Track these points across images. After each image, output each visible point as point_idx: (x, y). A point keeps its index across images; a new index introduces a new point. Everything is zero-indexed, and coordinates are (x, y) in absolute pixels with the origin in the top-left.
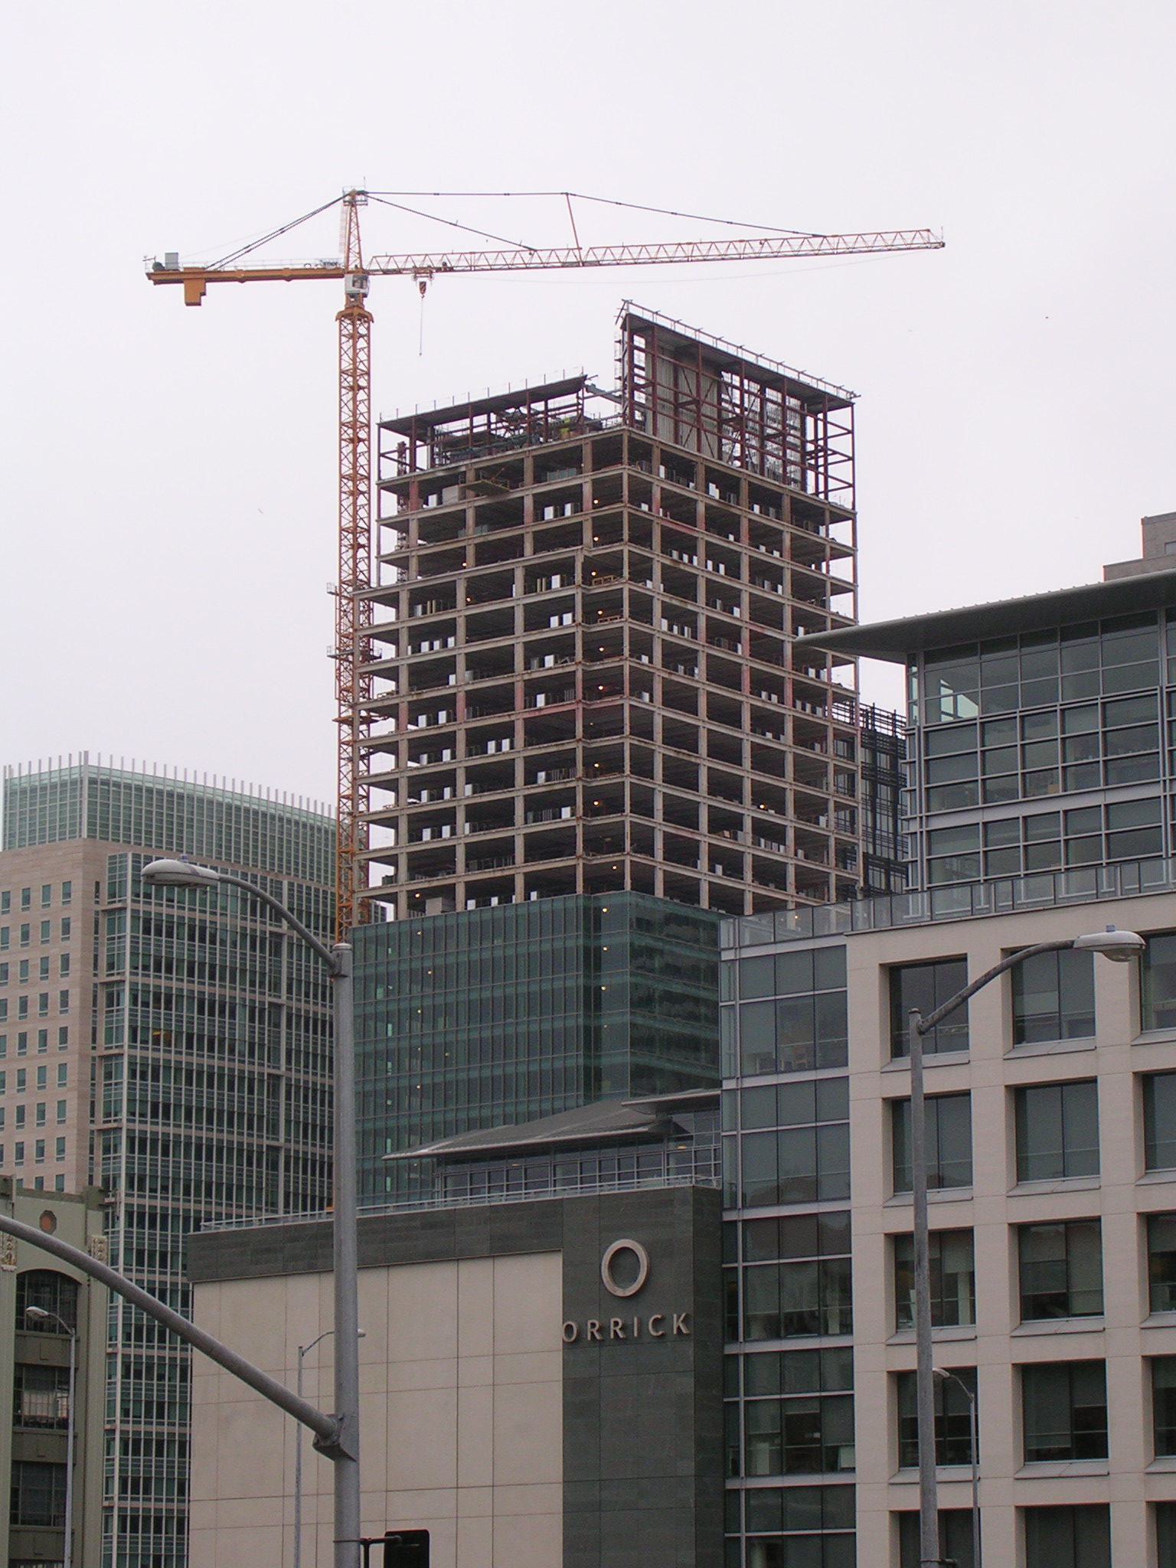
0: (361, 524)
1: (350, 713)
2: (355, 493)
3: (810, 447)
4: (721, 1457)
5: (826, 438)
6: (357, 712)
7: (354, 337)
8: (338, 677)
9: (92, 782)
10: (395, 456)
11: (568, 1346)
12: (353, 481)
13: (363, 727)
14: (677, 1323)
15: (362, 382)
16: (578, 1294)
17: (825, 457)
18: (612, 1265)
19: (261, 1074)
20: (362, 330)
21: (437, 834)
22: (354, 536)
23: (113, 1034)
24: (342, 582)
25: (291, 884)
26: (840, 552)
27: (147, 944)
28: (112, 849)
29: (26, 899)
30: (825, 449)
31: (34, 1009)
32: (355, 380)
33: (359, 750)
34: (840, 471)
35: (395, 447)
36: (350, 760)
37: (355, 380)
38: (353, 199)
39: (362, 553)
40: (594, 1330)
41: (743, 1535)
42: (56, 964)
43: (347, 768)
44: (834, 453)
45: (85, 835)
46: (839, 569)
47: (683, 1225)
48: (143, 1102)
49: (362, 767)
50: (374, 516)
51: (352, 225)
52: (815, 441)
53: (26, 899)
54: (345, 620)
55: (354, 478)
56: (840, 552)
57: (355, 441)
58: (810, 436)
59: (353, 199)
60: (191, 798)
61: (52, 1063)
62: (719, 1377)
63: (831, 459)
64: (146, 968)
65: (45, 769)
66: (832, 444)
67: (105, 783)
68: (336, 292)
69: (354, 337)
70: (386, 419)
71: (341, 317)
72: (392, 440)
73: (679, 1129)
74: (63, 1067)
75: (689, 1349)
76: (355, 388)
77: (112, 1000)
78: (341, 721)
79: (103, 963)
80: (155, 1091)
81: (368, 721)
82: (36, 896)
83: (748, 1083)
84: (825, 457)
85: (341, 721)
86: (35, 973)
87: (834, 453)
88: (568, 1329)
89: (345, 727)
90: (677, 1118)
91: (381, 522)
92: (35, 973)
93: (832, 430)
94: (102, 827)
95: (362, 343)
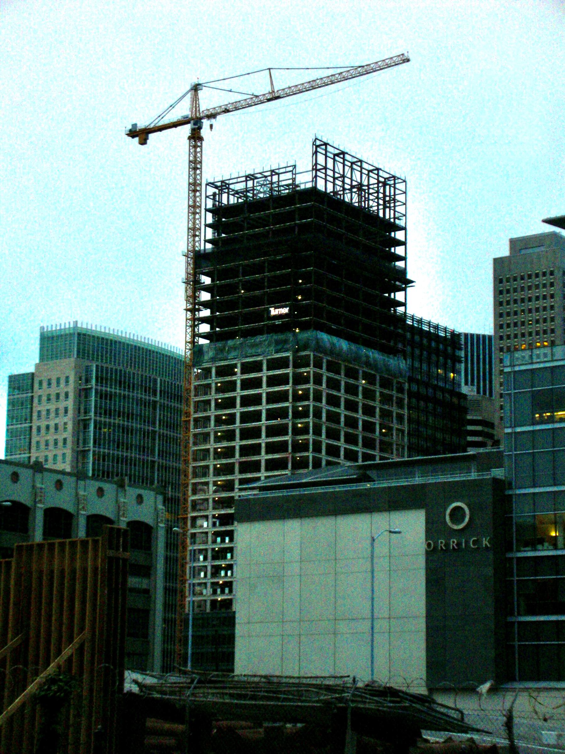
0: (197, 226)
1: (191, 307)
2: (195, 213)
3: (387, 199)
4: (503, 606)
5: (395, 195)
6: (194, 305)
7: (195, 147)
8: (186, 291)
9: (79, 334)
10: (212, 197)
11: (427, 553)
12: (194, 208)
13: (197, 313)
14: (485, 542)
15: (199, 166)
16: (433, 528)
17: (394, 203)
18: (451, 515)
19: (148, 460)
20: (199, 144)
21: (223, 541)
22: (194, 231)
23: (85, 442)
24: (188, 251)
25: (161, 380)
26: (399, 243)
27: (101, 403)
28: (86, 363)
29: (49, 384)
30: (394, 199)
31: (52, 430)
32: (195, 165)
33: (195, 321)
34: (400, 209)
35: (211, 194)
36: (191, 326)
37: (195, 165)
38: (196, 88)
39: (197, 239)
40: (443, 545)
41: (517, 643)
42: (62, 411)
43: (189, 330)
44: (398, 201)
45: (75, 356)
46: (399, 251)
47: (488, 498)
48: (99, 470)
49: (196, 330)
50: (203, 223)
51: (195, 99)
52: (390, 196)
53: (49, 384)
54: (189, 267)
55: (194, 206)
56: (399, 243)
57: (195, 191)
58: (388, 194)
59: (196, 88)
60: (120, 342)
61: (59, 453)
62: (503, 568)
63: (397, 181)
64: (100, 414)
65: (63, 327)
66: (397, 197)
67: (84, 335)
68: (186, 130)
69: (195, 147)
70: (209, 181)
71: (189, 138)
72: (211, 191)
73: (370, 477)
74: (64, 454)
75: (491, 556)
76: (195, 169)
77: (86, 426)
78: (187, 310)
79: (82, 411)
80: (104, 466)
81: (199, 310)
82: (54, 382)
83: (519, 430)
84: (394, 203)
85: (187, 310)
86: (52, 415)
87: (398, 201)
88: (429, 545)
89: (189, 313)
90: (368, 472)
91: (206, 225)
92: (52, 415)
93: (397, 192)
94: (82, 353)
95: (198, 149)
